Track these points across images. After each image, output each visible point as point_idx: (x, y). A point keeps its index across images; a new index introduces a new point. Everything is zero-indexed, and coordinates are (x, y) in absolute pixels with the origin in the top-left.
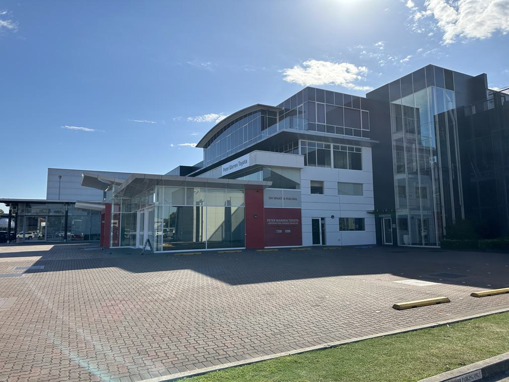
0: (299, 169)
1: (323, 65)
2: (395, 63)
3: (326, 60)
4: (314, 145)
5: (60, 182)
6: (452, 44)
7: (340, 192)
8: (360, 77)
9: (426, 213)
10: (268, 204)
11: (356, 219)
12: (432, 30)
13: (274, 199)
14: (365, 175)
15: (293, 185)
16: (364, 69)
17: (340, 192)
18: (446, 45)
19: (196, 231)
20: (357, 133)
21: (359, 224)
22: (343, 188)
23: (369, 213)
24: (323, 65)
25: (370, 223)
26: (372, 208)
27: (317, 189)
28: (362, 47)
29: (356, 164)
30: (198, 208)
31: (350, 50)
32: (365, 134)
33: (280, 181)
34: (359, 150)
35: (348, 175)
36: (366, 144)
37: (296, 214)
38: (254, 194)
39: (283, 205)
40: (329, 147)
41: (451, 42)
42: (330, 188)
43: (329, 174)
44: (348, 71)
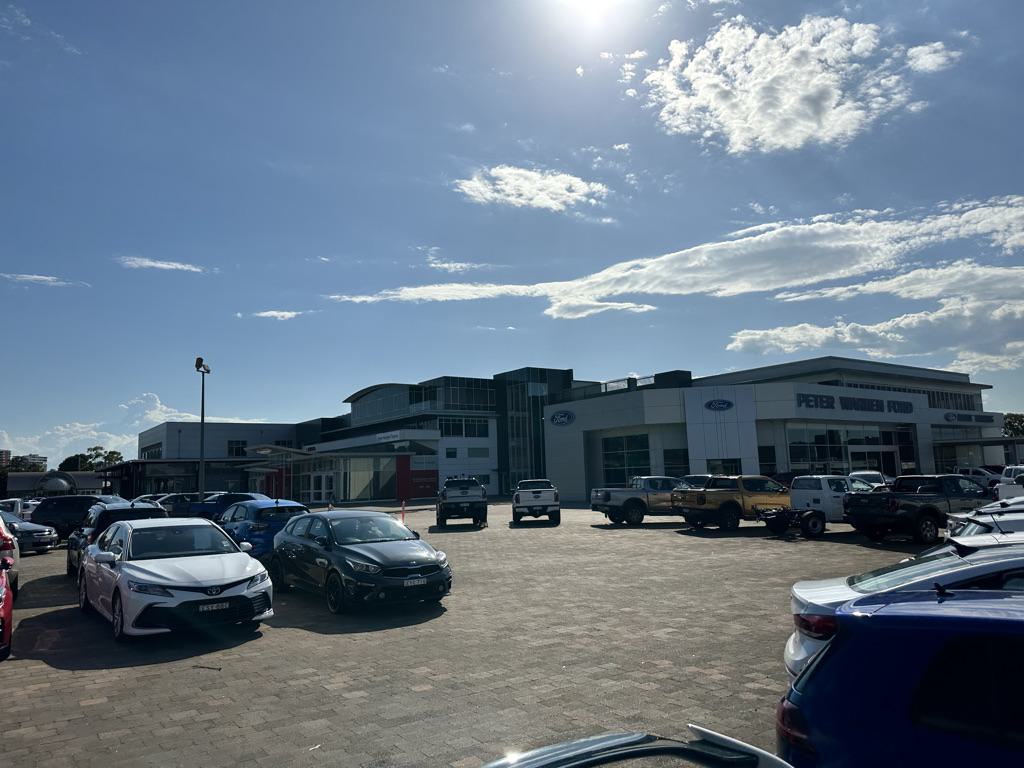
0: (437, 441)
1: (526, 178)
2: (655, 181)
3: (530, 168)
4: (449, 420)
5: (179, 451)
6: (745, 153)
7: (470, 455)
8: (593, 201)
9: (938, 415)
10: (414, 467)
11: (686, 452)
12: (709, 127)
13: (419, 463)
14: (490, 442)
15: (433, 453)
16: (598, 187)
17: (470, 455)
18: (735, 154)
19: (863, 409)
20: (485, 408)
21: (486, 479)
22: (473, 452)
23: (494, 470)
24: (526, 178)
25: (494, 478)
26: (496, 467)
27: (451, 454)
28: (595, 150)
29: (484, 433)
30: (345, 474)
31: (574, 154)
32: (492, 409)
33: (418, 448)
34: (486, 421)
35: (478, 442)
36: (492, 418)
37: (435, 473)
38: (403, 462)
39: (424, 468)
40: (461, 421)
41: (744, 148)
42: (462, 453)
43: (462, 443)
44: (570, 190)
